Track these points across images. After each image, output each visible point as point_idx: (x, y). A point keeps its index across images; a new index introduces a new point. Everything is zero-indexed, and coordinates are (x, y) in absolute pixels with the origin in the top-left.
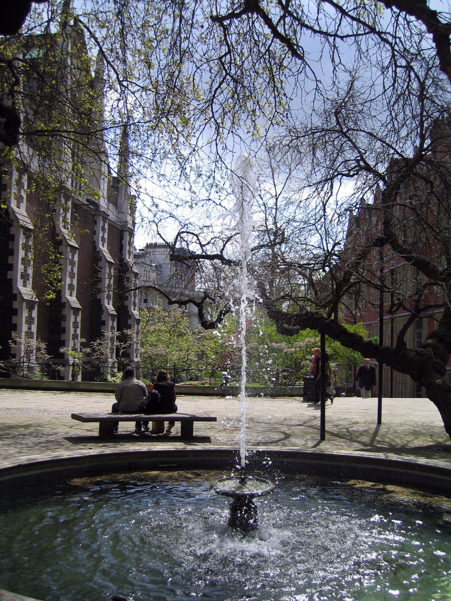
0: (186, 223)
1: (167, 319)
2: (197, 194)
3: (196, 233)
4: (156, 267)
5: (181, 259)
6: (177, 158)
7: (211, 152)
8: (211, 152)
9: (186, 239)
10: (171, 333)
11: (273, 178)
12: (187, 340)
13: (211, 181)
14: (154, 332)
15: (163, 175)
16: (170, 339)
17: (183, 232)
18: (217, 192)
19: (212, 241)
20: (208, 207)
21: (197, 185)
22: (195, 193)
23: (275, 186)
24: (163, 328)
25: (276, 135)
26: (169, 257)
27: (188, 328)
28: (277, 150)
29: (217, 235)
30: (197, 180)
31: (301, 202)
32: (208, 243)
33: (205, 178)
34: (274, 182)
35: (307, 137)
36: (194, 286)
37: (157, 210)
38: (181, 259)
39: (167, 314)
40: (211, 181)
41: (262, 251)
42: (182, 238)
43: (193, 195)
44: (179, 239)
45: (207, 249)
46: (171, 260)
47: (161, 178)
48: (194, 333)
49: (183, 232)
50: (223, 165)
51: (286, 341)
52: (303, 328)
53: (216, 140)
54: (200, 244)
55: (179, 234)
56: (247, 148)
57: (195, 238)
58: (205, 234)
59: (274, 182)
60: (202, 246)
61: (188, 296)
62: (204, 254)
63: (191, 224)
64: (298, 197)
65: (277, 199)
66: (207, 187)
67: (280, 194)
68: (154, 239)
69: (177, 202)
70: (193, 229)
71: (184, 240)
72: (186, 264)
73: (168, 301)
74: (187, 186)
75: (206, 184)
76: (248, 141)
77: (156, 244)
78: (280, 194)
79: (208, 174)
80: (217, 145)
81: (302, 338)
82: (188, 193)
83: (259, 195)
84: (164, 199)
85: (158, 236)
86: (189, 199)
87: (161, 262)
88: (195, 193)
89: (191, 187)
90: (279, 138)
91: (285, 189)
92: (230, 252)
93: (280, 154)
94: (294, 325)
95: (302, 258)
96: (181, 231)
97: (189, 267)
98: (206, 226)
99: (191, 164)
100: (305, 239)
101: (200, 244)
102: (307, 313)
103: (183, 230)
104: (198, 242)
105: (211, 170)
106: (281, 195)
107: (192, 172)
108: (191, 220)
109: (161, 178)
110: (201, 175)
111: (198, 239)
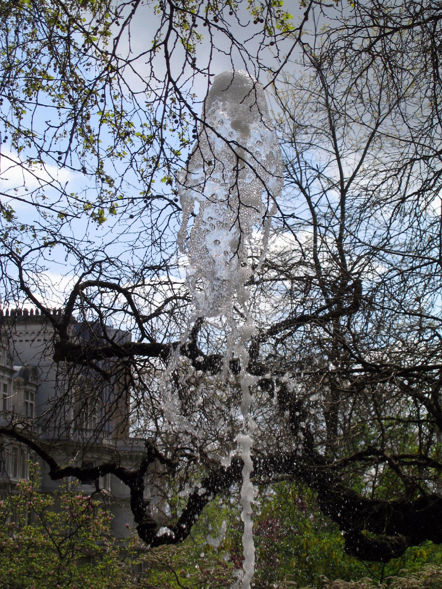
0: (98, 259)
1: (51, 514)
2: (117, 184)
3: (124, 284)
4: (24, 374)
5: (84, 357)
6: (66, 90)
7: (152, 75)
8: (152, 75)
9: (96, 302)
10: (63, 552)
11: (334, 136)
12: (106, 572)
13: (154, 150)
14: (17, 550)
15: (27, 134)
16: (59, 569)
17: (90, 284)
18: (170, 182)
19: (168, 307)
20: (155, 215)
21: (117, 161)
22: (111, 182)
23: (338, 159)
24: (41, 539)
25: (337, 24)
26: (51, 351)
27: (109, 538)
28: (338, 65)
29: (180, 289)
30: (119, 149)
31: (403, 199)
32: (158, 313)
33: (138, 143)
34: (336, 148)
35: (418, 28)
36: (125, 424)
37: (10, 225)
38: (84, 357)
39: (50, 501)
40: (154, 150)
41: (300, 333)
42: (84, 298)
43: (106, 186)
44: (78, 301)
45: (156, 327)
46: (57, 358)
47: (22, 141)
48: (123, 554)
49: (90, 284)
50: (186, 110)
51: (372, 575)
52: (416, 541)
53: (165, 43)
54: (136, 313)
55: (78, 289)
56: (249, 63)
57: (123, 299)
58: (148, 288)
59: (336, 148)
60: (140, 319)
61: (110, 451)
62: (146, 341)
63: (112, 263)
64: (396, 186)
65: (343, 192)
66: (144, 166)
67: (352, 179)
68: (12, 302)
69: (63, 205)
70: (115, 274)
71: (93, 306)
72: (98, 369)
73: (48, 469)
74: (92, 162)
75: (138, 158)
76: (252, 47)
77: (17, 312)
78: (352, 179)
79: (148, 133)
80: (167, 57)
81: (417, 566)
82: (91, 181)
83: (297, 182)
84: (28, 198)
85: (22, 293)
86: (93, 199)
87: (35, 363)
88: (111, 182)
89: (101, 165)
90: (345, 32)
91: (365, 165)
92: (218, 335)
93: (347, 75)
94: (390, 532)
95: (411, 352)
96: (84, 280)
97: (106, 377)
98: (151, 268)
99: (101, 105)
100: (418, 299)
101: (136, 313)
102: (426, 499)
103: (90, 277)
104: (130, 309)
105: (155, 121)
106: (356, 180)
107: (104, 125)
108: (112, 252)
109: (22, 141)
110: (128, 134)
111: (130, 302)
